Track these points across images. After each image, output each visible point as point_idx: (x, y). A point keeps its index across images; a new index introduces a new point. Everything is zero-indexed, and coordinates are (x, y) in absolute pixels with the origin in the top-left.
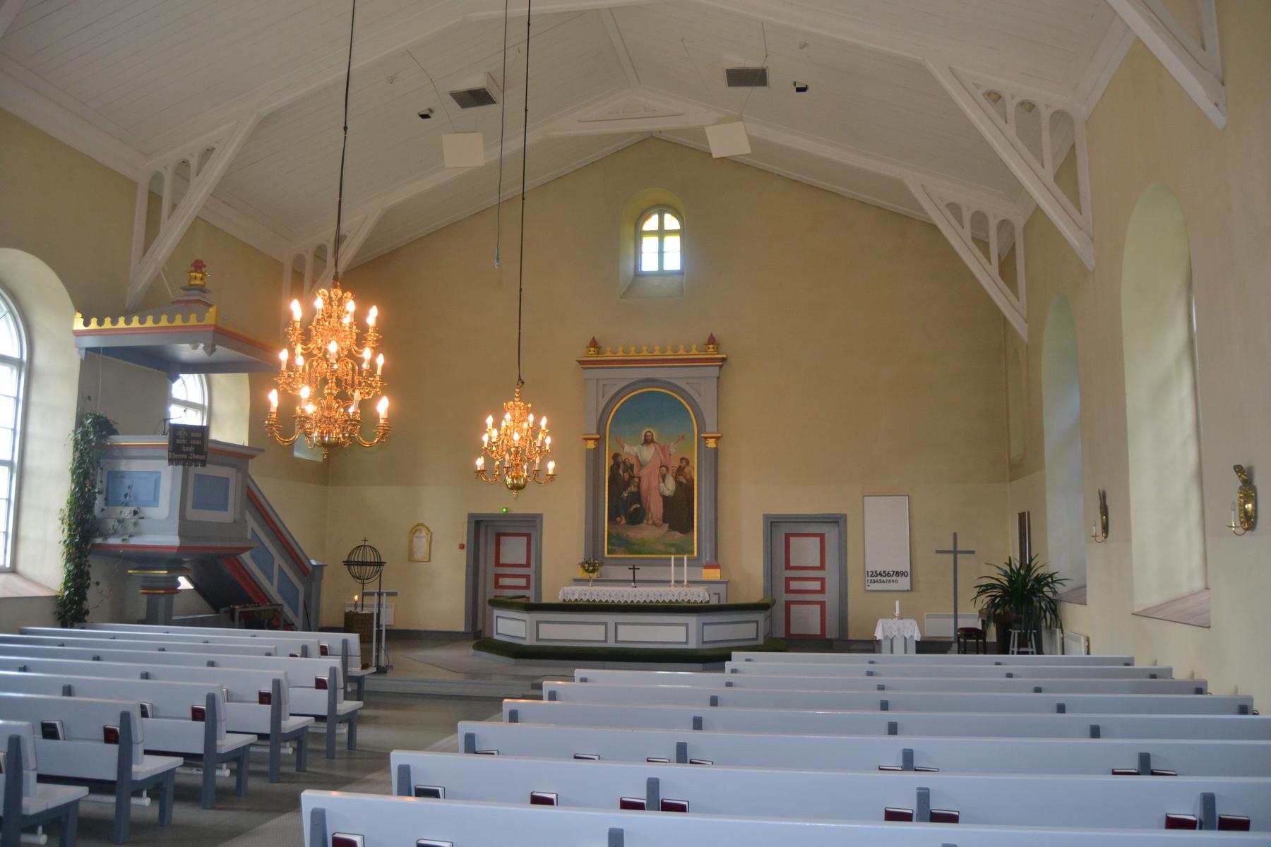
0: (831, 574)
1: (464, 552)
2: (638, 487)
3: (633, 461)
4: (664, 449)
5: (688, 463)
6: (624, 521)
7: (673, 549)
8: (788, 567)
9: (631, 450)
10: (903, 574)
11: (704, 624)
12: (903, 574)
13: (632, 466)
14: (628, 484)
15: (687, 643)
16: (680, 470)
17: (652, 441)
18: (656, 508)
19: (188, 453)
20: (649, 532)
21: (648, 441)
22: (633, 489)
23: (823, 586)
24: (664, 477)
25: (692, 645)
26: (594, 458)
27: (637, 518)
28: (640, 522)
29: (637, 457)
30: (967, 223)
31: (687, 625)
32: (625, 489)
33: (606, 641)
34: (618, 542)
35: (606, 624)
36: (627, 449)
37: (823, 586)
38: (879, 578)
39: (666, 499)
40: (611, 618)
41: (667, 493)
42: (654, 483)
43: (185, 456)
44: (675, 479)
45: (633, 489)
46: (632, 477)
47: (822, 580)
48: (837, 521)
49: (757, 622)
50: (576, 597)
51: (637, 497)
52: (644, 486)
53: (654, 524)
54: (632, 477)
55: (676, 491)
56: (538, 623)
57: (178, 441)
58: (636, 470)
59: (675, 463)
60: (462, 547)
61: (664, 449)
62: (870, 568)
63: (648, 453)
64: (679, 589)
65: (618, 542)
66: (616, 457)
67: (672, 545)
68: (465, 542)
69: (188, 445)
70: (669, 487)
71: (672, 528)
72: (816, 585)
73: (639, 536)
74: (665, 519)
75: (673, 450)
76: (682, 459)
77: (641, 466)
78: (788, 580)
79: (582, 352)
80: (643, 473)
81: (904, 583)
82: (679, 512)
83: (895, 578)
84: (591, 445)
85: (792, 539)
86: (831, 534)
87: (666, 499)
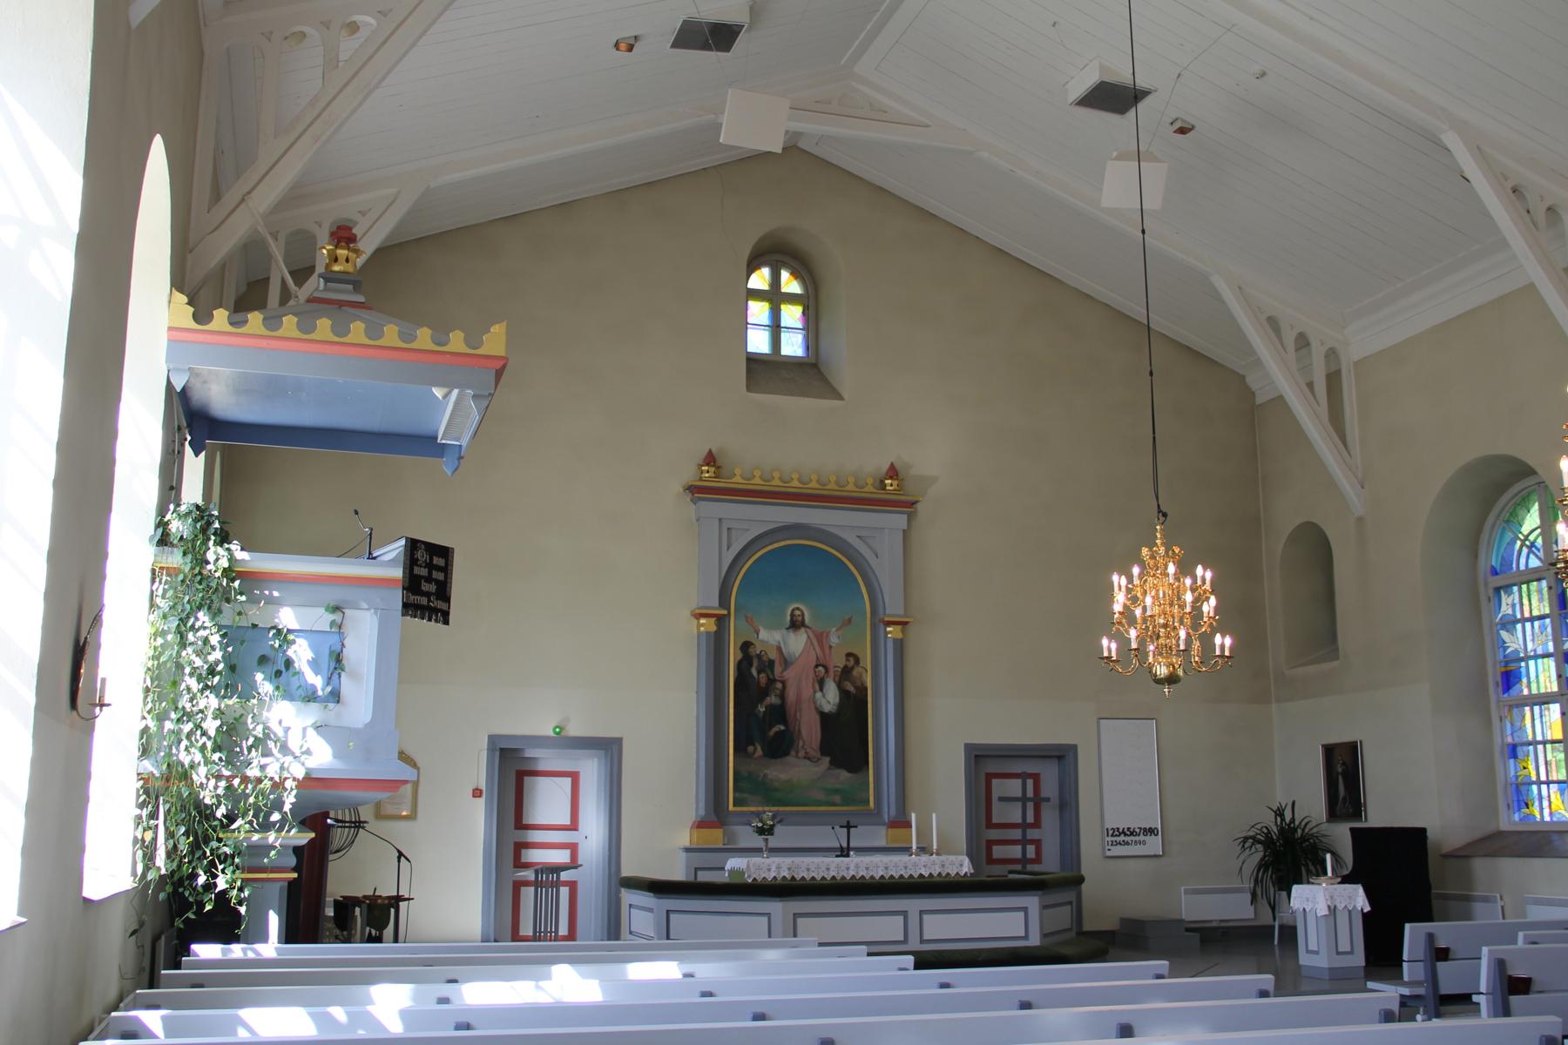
0: (1049, 833)
1: (481, 802)
2: (782, 696)
3: (773, 655)
4: (821, 638)
5: (857, 661)
6: (759, 752)
7: (837, 798)
8: (990, 825)
9: (769, 637)
10: (1151, 831)
11: (796, 916)
12: (1151, 831)
13: (771, 663)
14: (764, 692)
15: (1026, 937)
16: (846, 672)
17: (803, 624)
18: (809, 731)
19: (428, 595)
20: (802, 770)
21: (796, 624)
22: (773, 699)
23: (574, 856)
24: (821, 683)
25: (1035, 940)
26: (717, 642)
27: (780, 747)
28: (787, 754)
29: (779, 649)
30: (1291, 347)
31: (1025, 910)
32: (761, 700)
33: (1026, 937)
34: (751, 787)
35: (905, 913)
36: (764, 634)
37: (574, 856)
38: (1122, 838)
39: (825, 718)
40: (913, 904)
41: (827, 708)
42: (807, 692)
43: (424, 601)
44: (839, 686)
45: (773, 699)
46: (772, 681)
47: (573, 848)
48: (1063, 756)
49: (1025, 910)
50: (852, 873)
51: (779, 713)
52: (791, 695)
53: (807, 757)
54: (772, 681)
55: (841, 706)
56: (796, 916)
57: (417, 570)
58: (778, 669)
59: (838, 661)
60: (477, 793)
61: (821, 638)
62: (1110, 825)
63: (796, 643)
64: (924, 858)
65: (751, 787)
66: (746, 646)
67: (837, 791)
68: (483, 786)
69: (429, 579)
70: (830, 698)
71: (836, 763)
72: (562, 857)
73: (783, 777)
74: (825, 749)
75: (834, 640)
76: (849, 655)
77: (786, 663)
78: (990, 843)
79: (688, 474)
80: (790, 674)
81: (1154, 845)
82: (847, 737)
83: (1142, 838)
84: (708, 625)
85: (995, 782)
86: (1049, 774)
87: (825, 718)
